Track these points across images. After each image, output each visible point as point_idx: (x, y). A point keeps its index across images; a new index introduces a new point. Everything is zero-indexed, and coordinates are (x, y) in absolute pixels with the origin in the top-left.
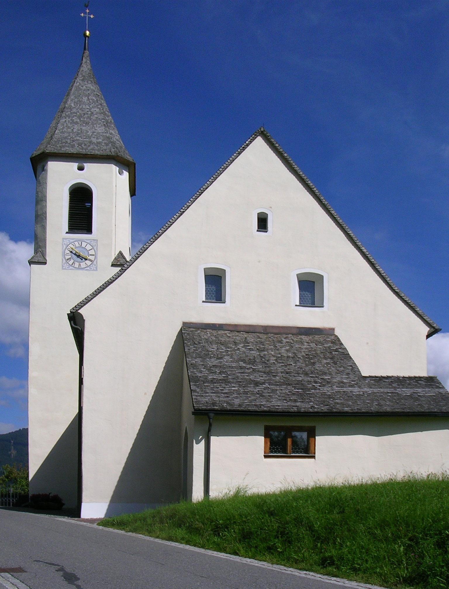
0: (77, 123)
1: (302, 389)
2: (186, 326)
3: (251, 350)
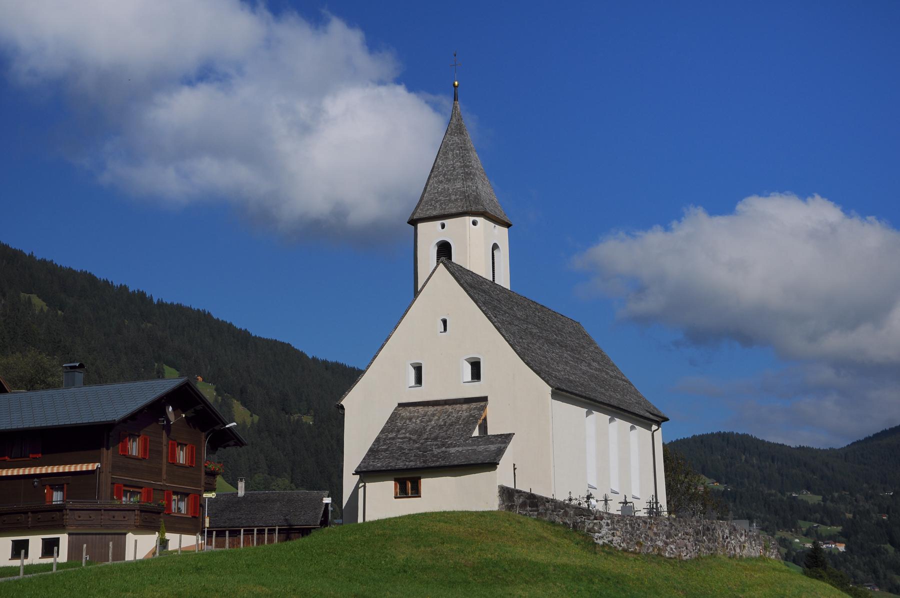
0: (441, 182)
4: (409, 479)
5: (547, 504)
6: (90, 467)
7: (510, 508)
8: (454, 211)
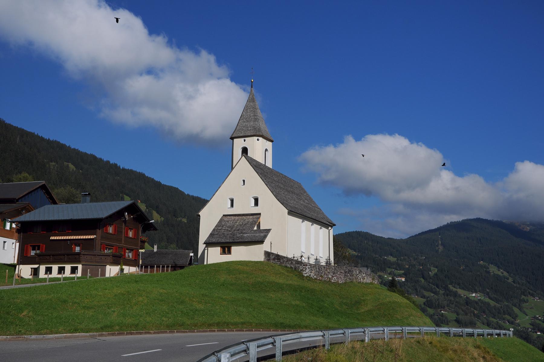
2: (224, 215)
6: (92, 237)
7: (269, 260)
8: (249, 134)
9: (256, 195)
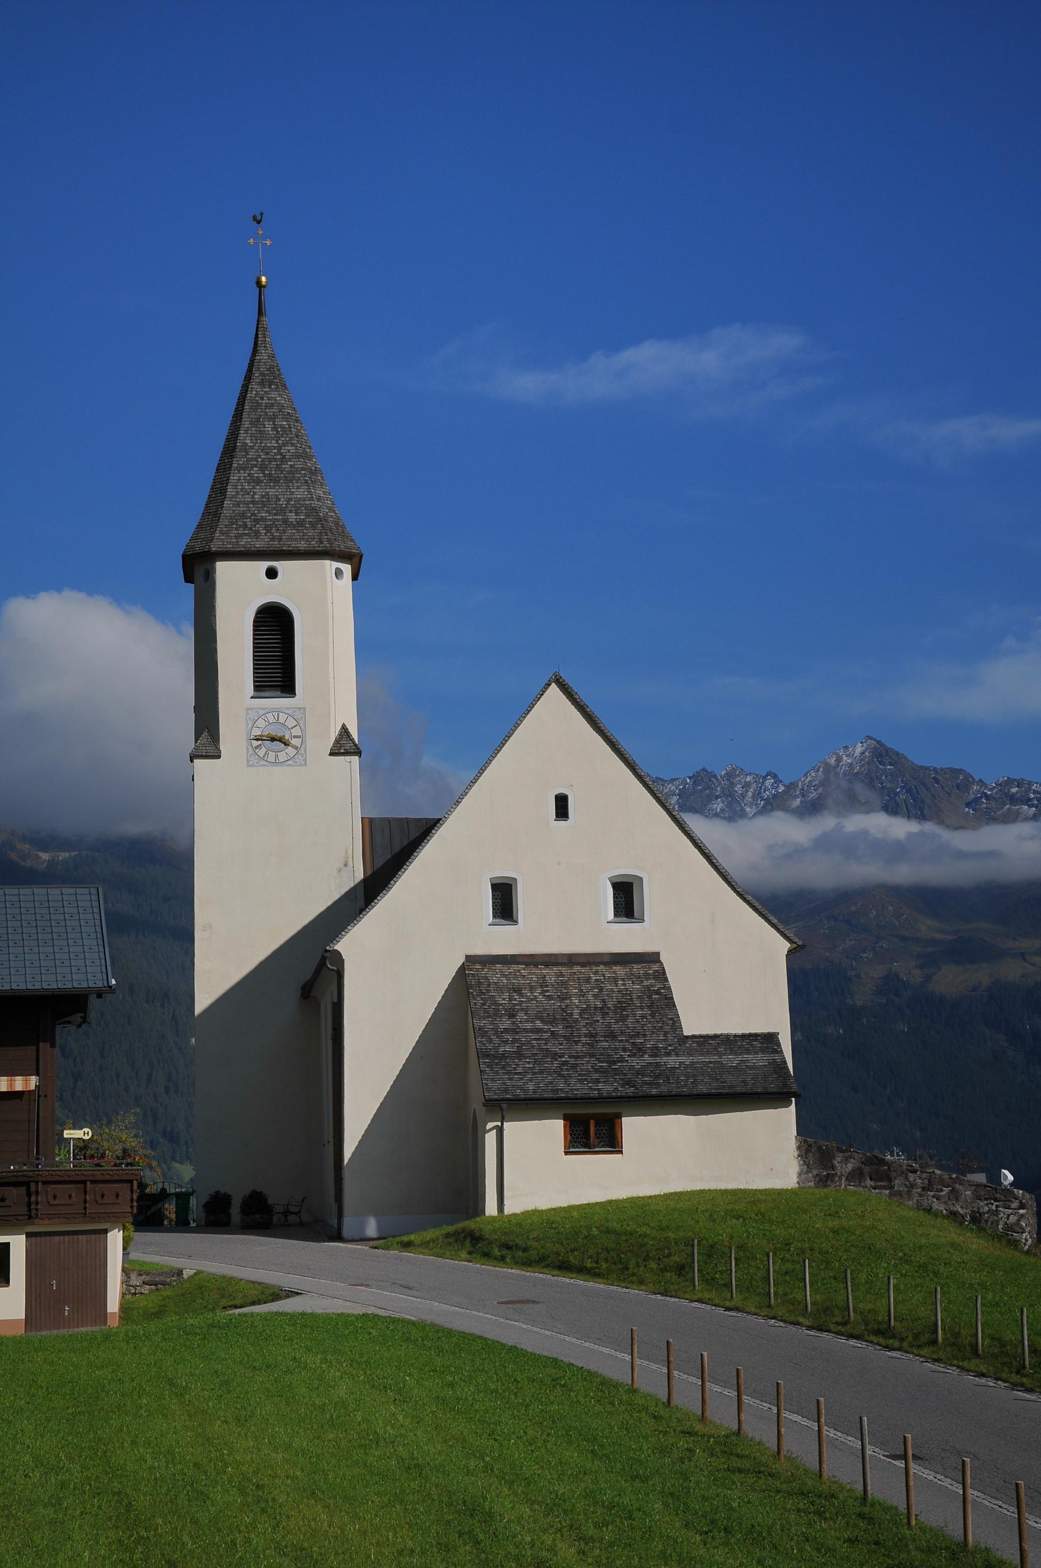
0: (258, 482)
1: (607, 1062)
3: (550, 998)
4: (594, 1116)
5: (912, 1177)
6: (19, 1084)
7: (824, 1181)
8: (302, 545)
9: (624, 870)
